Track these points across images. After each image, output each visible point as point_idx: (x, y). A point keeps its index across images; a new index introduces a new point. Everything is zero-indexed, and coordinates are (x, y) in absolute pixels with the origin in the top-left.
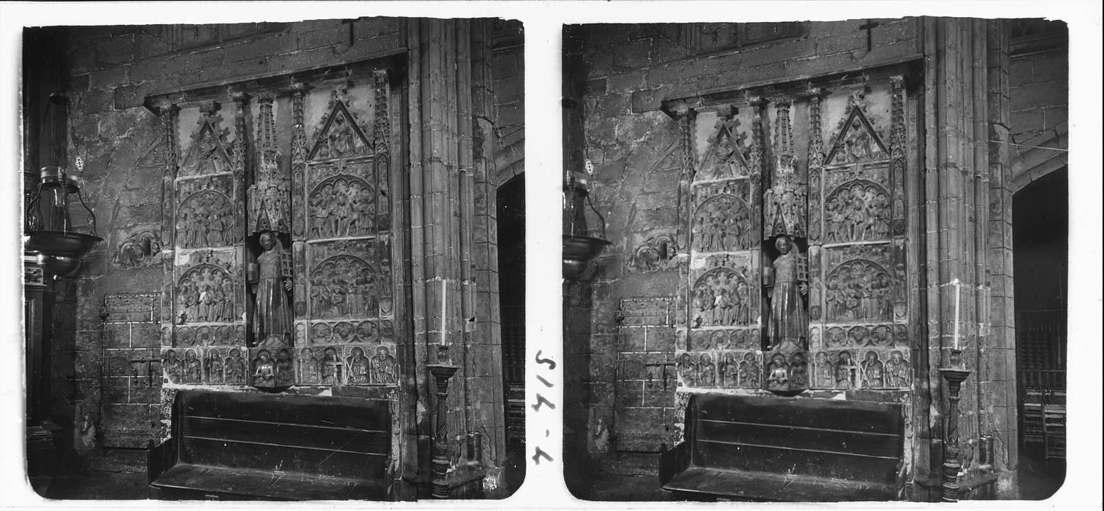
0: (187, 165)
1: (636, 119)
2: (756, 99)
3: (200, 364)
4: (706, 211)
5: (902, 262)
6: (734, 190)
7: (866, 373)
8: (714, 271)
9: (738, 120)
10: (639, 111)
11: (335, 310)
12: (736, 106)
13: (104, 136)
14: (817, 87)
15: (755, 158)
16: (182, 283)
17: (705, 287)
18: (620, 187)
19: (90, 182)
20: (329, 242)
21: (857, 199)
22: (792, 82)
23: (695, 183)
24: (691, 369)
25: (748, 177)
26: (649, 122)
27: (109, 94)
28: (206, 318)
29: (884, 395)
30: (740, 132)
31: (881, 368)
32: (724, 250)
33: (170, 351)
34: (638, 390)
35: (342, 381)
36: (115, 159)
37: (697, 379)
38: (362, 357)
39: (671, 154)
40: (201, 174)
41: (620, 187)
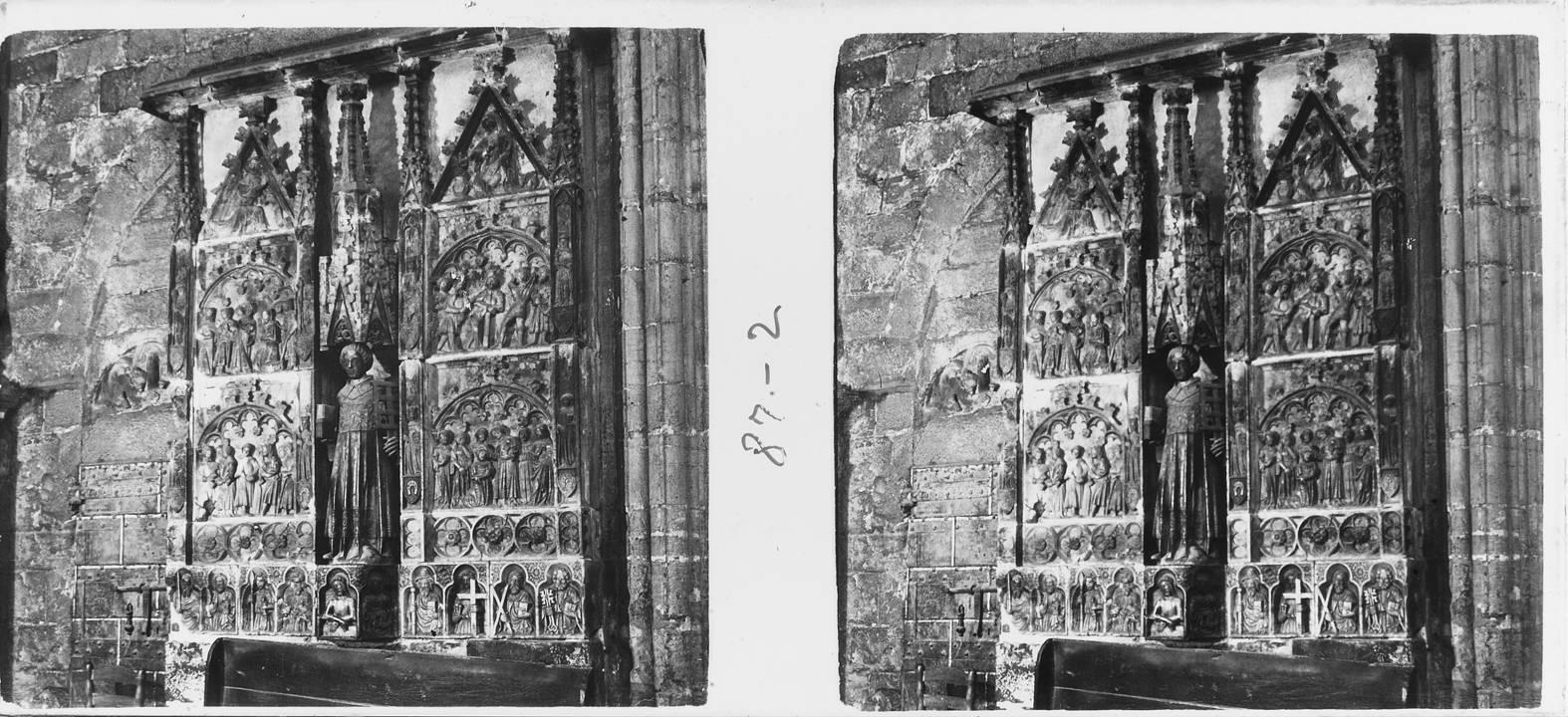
0: (1045, 222)
1: (936, 127)
2: (1132, 88)
3: (1063, 597)
4: (222, 296)
5: (571, 390)
6: (268, 256)
7: (505, 607)
8: (1063, 413)
9: (275, 121)
10: (111, 108)
11: (475, 492)
12: (272, 97)
13: (911, 168)
14: (1238, 61)
15: (1130, 200)
16: (207, 441)
17: (219, 442)
18: (78, 252)
19: (55, 250)
20: (466, 361)
21: (493, 266)
22: (1188, 57)
23: (202, 244)
24: (193, 597)
25: (292, 231)
26: (958, 134)
27: (91, 84)
28: (1077, 510)
29: (536, 651)
30: (1107, 148)
31: (530, 597)
32: (1081, 374)
33: (183, 571)
34: (110, 638)
35: (1312, 628)
36: (928, 210)
37: (1034, 619)
38: (1346, 583)
39: (995, 190)
40: (240, 235)
41: (78, 252)
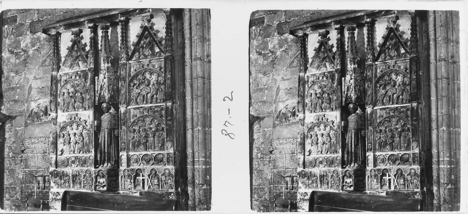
0: (312, 66)
1: (279, 38)
2: (338, 26)
3: (317, 178)
4: (66, 88)
5: (170, 116)
6: (80, 76)
7: (151, 181)
8: (317, 123)
9: (82, 36)
10: (33, 32)
11: (142, 147)
12: (81, 29)
13: (272, 50)
14: (369, 18)
15: (337, 60)
16: (62, 132)
17: (65, 132)
18: (23, 75)
19: (16, 75)
20: (139, 108)
21: (147, 80)
22: (355, 17)
23: (60, 73)
24: (58, 178)
25: (87, 69)
26: (286, 40)
27: (27, 25)
28: (321, 152)
29: (160, 194)
30: (330, 44)
31: (158, 178)
32: (323, 112)
33: (55, 170)
34: (33, 190)
35: (391, 188)
36: (277, 63)
37: (309, 185)
38: (402, 174)
39: (297, 57)
40: (72, 70)
41: (23, 75)
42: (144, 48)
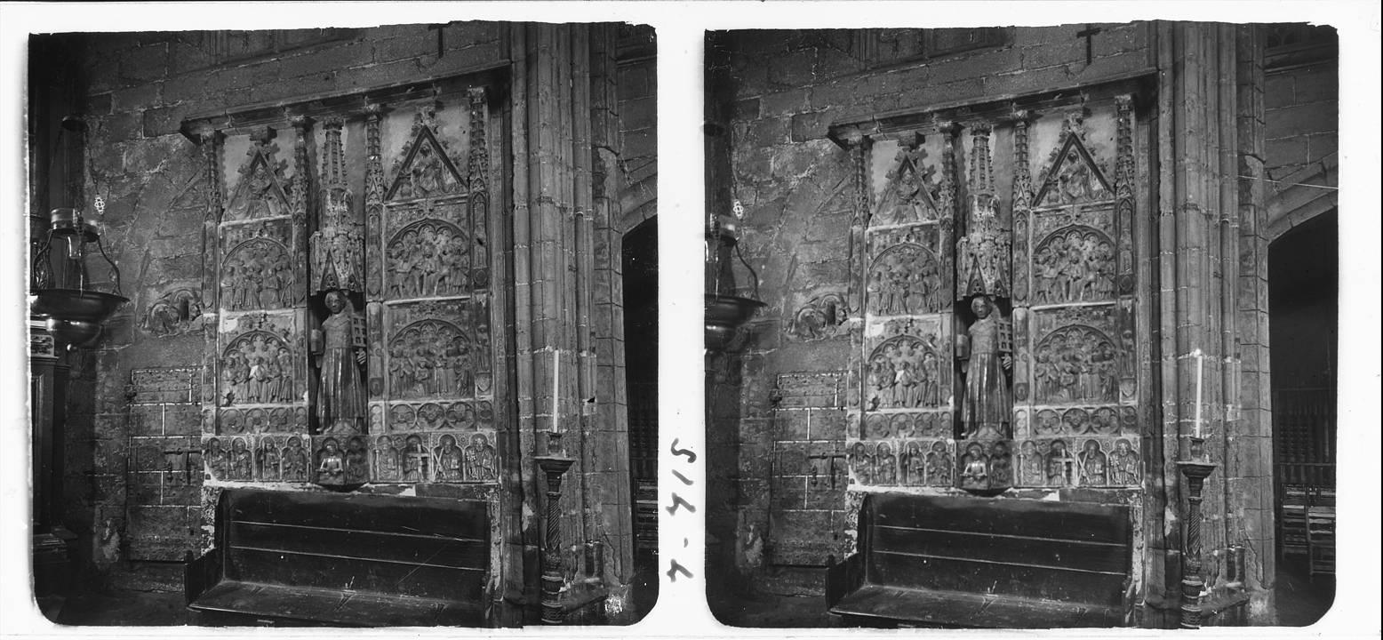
0: (234, 207)
1: (797, 149)
2: (947, 124)
3: (250, 456)
4: (885, 265)
5: (1129, 329)
6: (919, 238)
7: (1085, 467)
8: (894, 339)
9: (924, 150)
10: (800, 139)
11: (420, 388)
12: (923, 133)
13: (130, 170)
14: (1023, 109)
15: (946, 198)
16: (228, 354)
17: (883, 360)
18: (776, 234)
19: (113, 228)
20: (412, 303)
21: (1074, 249)
22: (992, 103)
23: (870, 229)
24: (865, 462)
25: (937, 221)
26: (813, 153)
27: (137, 117)
28: (258, 398)
29: (1107, 495)
30: (927, 166)
31: (1103, 460)
32: (907, 313)
33: (214, 440)
34: (800, 489)
35: (429, 477)
36: (144, 199)
37: (873, 475)
38: (454, 448)
39: (841, 193)
40: (252, 218)
41: (776, 234)
42: (1067, 180)
